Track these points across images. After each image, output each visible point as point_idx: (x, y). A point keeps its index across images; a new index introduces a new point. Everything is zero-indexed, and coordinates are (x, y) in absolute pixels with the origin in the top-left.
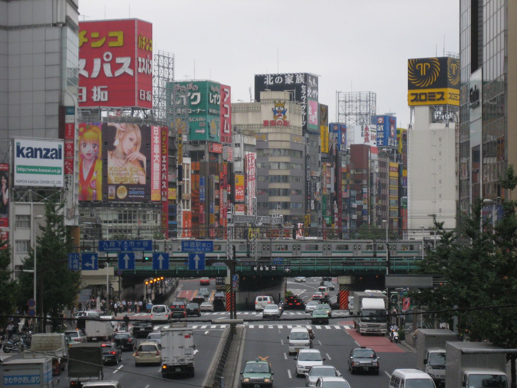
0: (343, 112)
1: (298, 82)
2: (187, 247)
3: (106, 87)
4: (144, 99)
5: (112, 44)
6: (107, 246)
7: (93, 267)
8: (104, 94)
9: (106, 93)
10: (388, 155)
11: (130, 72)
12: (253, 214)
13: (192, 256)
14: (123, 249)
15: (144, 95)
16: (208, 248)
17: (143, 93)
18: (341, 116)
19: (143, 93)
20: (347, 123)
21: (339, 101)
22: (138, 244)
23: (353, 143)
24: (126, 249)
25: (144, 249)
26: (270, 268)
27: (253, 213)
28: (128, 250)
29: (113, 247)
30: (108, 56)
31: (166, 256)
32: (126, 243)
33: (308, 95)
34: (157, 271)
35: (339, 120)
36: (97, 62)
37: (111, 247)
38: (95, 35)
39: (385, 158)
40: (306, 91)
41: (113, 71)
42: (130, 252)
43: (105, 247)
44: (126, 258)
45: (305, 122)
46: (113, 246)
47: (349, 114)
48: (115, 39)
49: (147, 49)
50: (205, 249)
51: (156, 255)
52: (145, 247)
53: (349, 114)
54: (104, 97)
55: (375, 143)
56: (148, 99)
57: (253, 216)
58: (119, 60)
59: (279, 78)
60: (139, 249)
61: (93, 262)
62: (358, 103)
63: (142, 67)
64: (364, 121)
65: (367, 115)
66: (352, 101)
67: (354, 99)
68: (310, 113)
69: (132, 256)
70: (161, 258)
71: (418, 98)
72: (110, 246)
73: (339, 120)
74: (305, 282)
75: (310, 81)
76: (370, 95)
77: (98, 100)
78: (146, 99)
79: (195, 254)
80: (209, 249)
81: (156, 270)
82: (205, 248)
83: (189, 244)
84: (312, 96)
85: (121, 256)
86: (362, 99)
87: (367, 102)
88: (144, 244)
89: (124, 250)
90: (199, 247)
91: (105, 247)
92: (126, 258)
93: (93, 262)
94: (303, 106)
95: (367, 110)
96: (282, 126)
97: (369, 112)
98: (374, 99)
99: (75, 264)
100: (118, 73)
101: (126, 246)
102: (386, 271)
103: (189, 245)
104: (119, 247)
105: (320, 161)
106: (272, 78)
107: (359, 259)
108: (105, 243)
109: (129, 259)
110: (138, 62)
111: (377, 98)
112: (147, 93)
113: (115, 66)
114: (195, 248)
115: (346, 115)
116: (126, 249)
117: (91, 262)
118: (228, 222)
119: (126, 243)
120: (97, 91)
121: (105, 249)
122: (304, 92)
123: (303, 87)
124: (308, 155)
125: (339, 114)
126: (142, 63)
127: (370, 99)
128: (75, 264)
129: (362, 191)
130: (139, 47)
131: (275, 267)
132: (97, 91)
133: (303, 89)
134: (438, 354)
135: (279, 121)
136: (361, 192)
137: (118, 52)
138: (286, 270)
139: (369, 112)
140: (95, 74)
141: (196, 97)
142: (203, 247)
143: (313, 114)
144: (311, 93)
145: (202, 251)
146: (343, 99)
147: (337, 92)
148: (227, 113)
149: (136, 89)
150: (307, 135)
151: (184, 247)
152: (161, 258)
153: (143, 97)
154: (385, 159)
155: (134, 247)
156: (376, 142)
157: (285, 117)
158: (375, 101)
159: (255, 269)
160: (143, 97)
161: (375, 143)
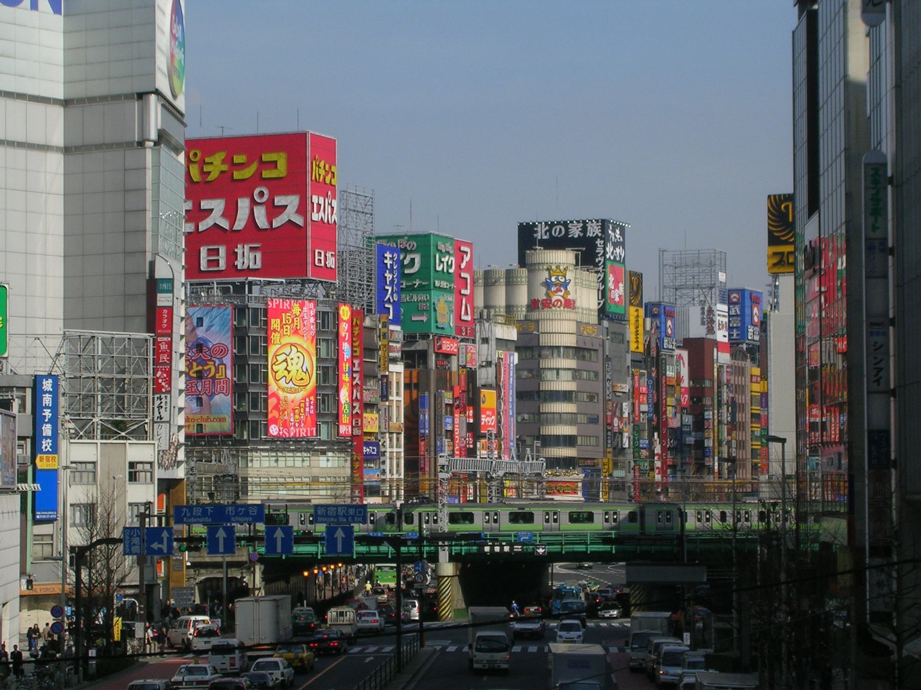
1: (591, 235)
2: (322, 516)
4: (323, 264)
5: (266, 174)
6: (189, 515)
7: (165, 551)
9: (259, 255)
11: (299, 220)
15: (322, 258)
16: (359, 517)
17: (320, 254)
19: (320, 254)
20: (678, 302)
25: (251, 519)
29: (199, 517)
30: (261, 194)
33: (608, 256)
36: (243, 204)
37: (195, 517)
38: (239, 159)
40: (604, 249)
41: (270, 216)
43: (185, 515)
45: (602, 302)
48: (274, 164)
49: (328, 181)
50: (353, 519)
52: (252, 516)
55: (725, 336)
58: (279, 201)
59: (558, 227)
62: (696, 269)
63: (318, 211)
68: (611, 285)
71: (785, 259)
75: (610, 232)
77: (245, 267)
78: (326, 265)
79: (338, 527)
84: (615, 257)
88: (250, 511)
90: (344, 516)
91: (185, 515)
94: (599, 275)
96: (562, 308)
98: (723, 262)
99: (134, 544)
100: (277, 223)
104: (209, 517)
106: (547, 228)
108: (184, 509)
109: (344, 536)
110: (313, 203)
113: (274, 210)
114: (337, 516)
117: (161, 542)
121: (185, 519)
122: (600, 250)
123: (598, 242)
126: (319, 205)
128: (134, 544)
130: (313, 178)
133: (599, 245)
135: (558, 300)
137: (279, 186)
138: (538, 551)
140: (240, 225)
141: (413, 260)
143: (617, 287)
144: (612, 253)
146: (670, 262)
148: (466, 288)
149: (309, 247)
150: (606, 323)
153: (320, 261)
154: (743, 363)
155: (234, 516)
156: (727, 334)
157: (567, 293)
159: (487, 549)
160: (320, 261)
161: (725, 336)
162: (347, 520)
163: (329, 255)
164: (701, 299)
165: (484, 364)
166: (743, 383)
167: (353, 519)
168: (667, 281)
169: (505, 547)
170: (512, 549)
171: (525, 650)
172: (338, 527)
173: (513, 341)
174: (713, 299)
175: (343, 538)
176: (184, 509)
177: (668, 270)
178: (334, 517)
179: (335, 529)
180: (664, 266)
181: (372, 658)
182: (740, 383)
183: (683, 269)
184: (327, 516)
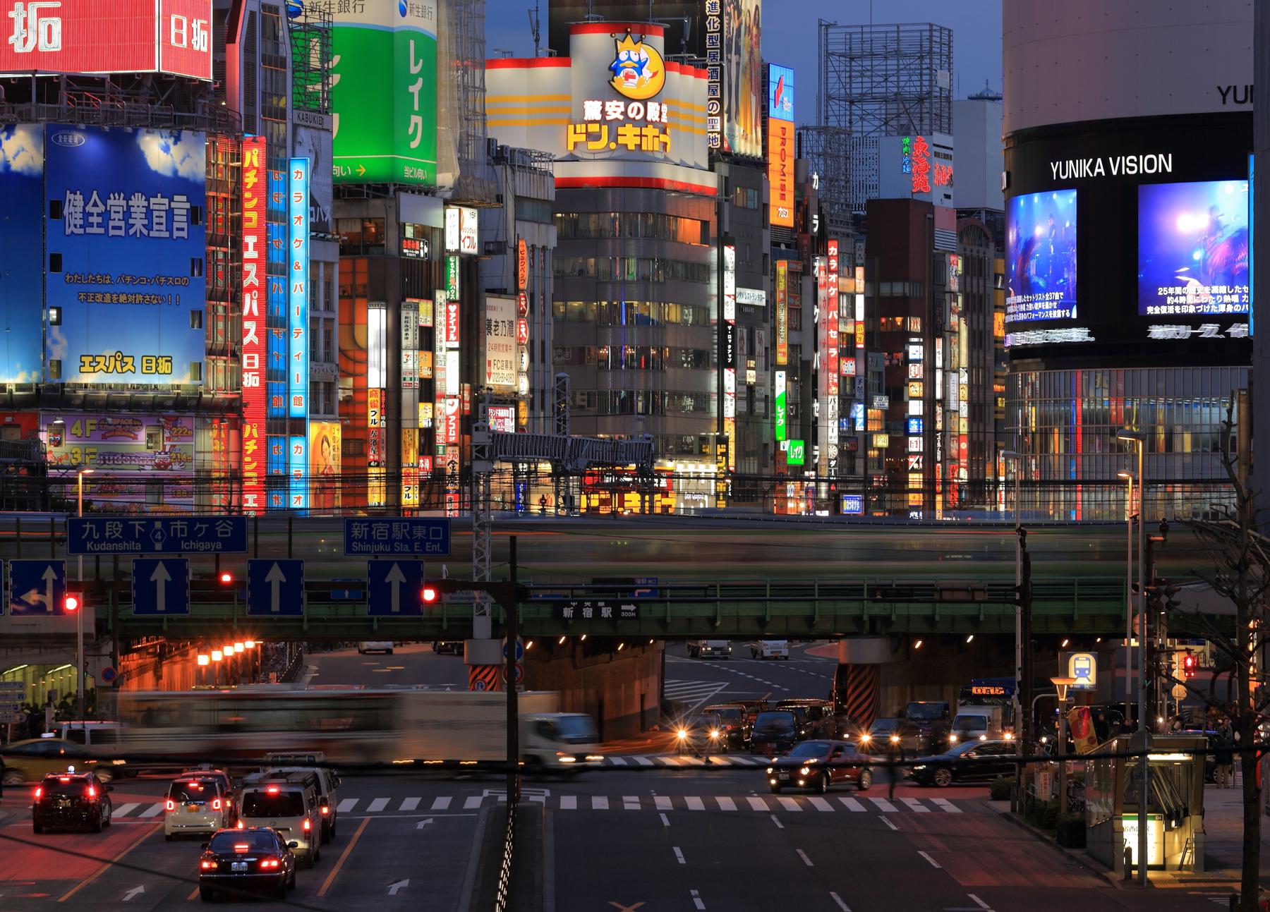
0: (843, 91)
2: (362, 541)
3: (58, 5)
8: (50, 27)
9: (57, 23)
10: (989, 234)
12: (559, 430)
13: (379, 570)
14: (148, 546)
16: (434, 542)
17: (179, 24)
18: (834, 106)
19: (179, 24)
20: (857, 126)
21: (828, 55)
22: (200, 529)
23: (874, 195)
24: (158, 546)
25: (219, 545)
26: (617, 612)
27: (559, 426)
28: (165, 549)
29: (117, 540)
31: (292, 568)
32: (158, 525)
34: (378, 620)
35: (827, 118)
37: (110, 541)
39: (980, 245)
42: (173, 556)
43: (90, 538)
44: (161, 575)
46: (117, 535)
47: (862, 98)
50: (422, 546)
51: (259, 569)
52: (221, 540)
53: (862, 98)
54: (50, 41)
56: (196, 48)
57: (556, 436)
60: (203, 546)
61: (50, 585)
62: (892, 62)
64: (911, 120)
65: (921, 100)
66: (872, 55)
67: (878, 48)
69: (177, 569)
70: (276, 576)
72: (107, 534)
73: (827, 118)
74: (786, 658)
76: (931, 36)
77: (29, 48)
78: (190, 45)
80: (437, 547)
81: (375, 617)
82: (423, 543)
83: (371, 529)
85: (145, 569)
86: (905, 48)
87: (921, 58)
88: (219, 529)
89: (153, 549)
90: (404, 540)
91: (90, 538)
92: (161, 575)
93: (50, 585)
95: (921, 86)
97: (930, 93)
98: (945, 48)
101: (158, 536)
102: (1014, 617)
103: (370, 532)
105: (766, 255)
107: (738, 596)
111: (955, 44)
112: (194, 25)
114: (390, 541)
115: (852, 103)
116: (158, 546)
118: (477, 458)
119: (158, 525)
120: (26, 20)
121: (89, 545)
124: (726, 233)
125: (829, 97)
127: (931, 48)
129: (907, 354)
131: (632, 607)
132: (26, 20)
134: (165, 718)
136: (901, 355)
139: (930, 93)
142: (417, 540)
145: (413, 552)
146: (840, 48)
147: (820, 25)
151: (354, 540)
152: (276, 576)
153: (179, 38)
154: (981, 249)
155: (186, 540)
158: (949, 57)
160: (179, 38)
162: (411, 547)
163: (196, 25)
164: (902, 122)
165: (491, 247)
166: (981, 291)
167: (422, 546)
168: (835, 88)
169: (604, 610)
170: (617, 612)
171: (615, 800)
172: (158, 561)
173: (548, 201)
174: (926, 122)
175: (401, 583)
176: (88, 526)
177: (836, 64)
178: (384, 542)
179: (387, 566)
180: (828, 55)
181: (430, 821)
182: (975, 290)
183: (867, 63)
184: (370, 540)
